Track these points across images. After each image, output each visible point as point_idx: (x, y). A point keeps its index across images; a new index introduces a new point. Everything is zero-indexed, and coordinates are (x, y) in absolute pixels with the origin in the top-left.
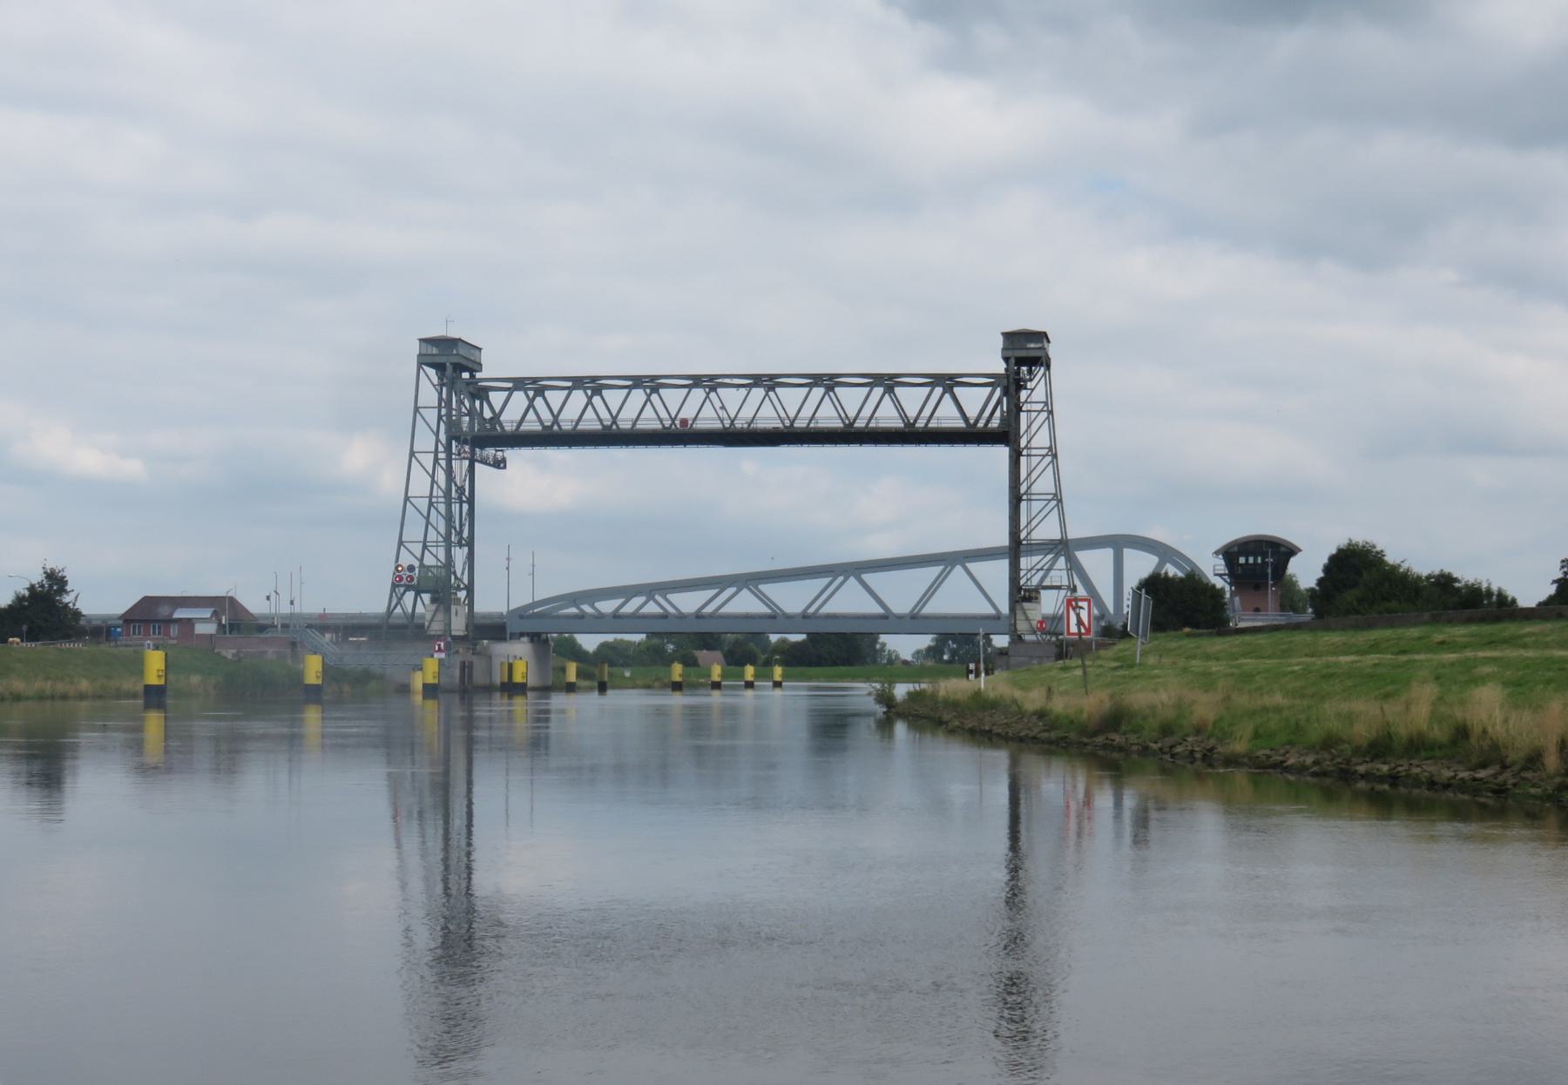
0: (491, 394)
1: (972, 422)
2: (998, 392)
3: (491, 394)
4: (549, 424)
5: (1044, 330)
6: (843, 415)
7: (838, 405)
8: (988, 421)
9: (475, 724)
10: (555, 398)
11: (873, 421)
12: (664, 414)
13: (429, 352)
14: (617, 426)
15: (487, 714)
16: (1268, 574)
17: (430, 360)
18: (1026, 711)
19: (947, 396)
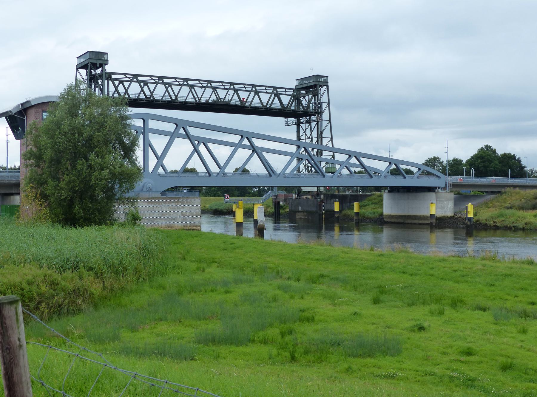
0: (124, 82)
1: (265, 105)
2: (273, 95)
3: (124, 82)
4: (149, 97)
5: (109, 63)
6: (270, 102)
7: (217, 95)
8: (290, 107)
9: (411, 307)
10: (176, 88)
11: (164, 97)
12: (172, 94)
13: (306, 83)
14: (154, 98)
15: (81, 394)
16: (446, 169)
17: (80, 66)
18: (263, 344)
19: (256, 96)
